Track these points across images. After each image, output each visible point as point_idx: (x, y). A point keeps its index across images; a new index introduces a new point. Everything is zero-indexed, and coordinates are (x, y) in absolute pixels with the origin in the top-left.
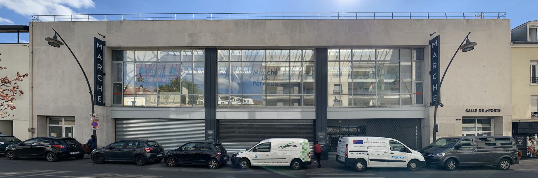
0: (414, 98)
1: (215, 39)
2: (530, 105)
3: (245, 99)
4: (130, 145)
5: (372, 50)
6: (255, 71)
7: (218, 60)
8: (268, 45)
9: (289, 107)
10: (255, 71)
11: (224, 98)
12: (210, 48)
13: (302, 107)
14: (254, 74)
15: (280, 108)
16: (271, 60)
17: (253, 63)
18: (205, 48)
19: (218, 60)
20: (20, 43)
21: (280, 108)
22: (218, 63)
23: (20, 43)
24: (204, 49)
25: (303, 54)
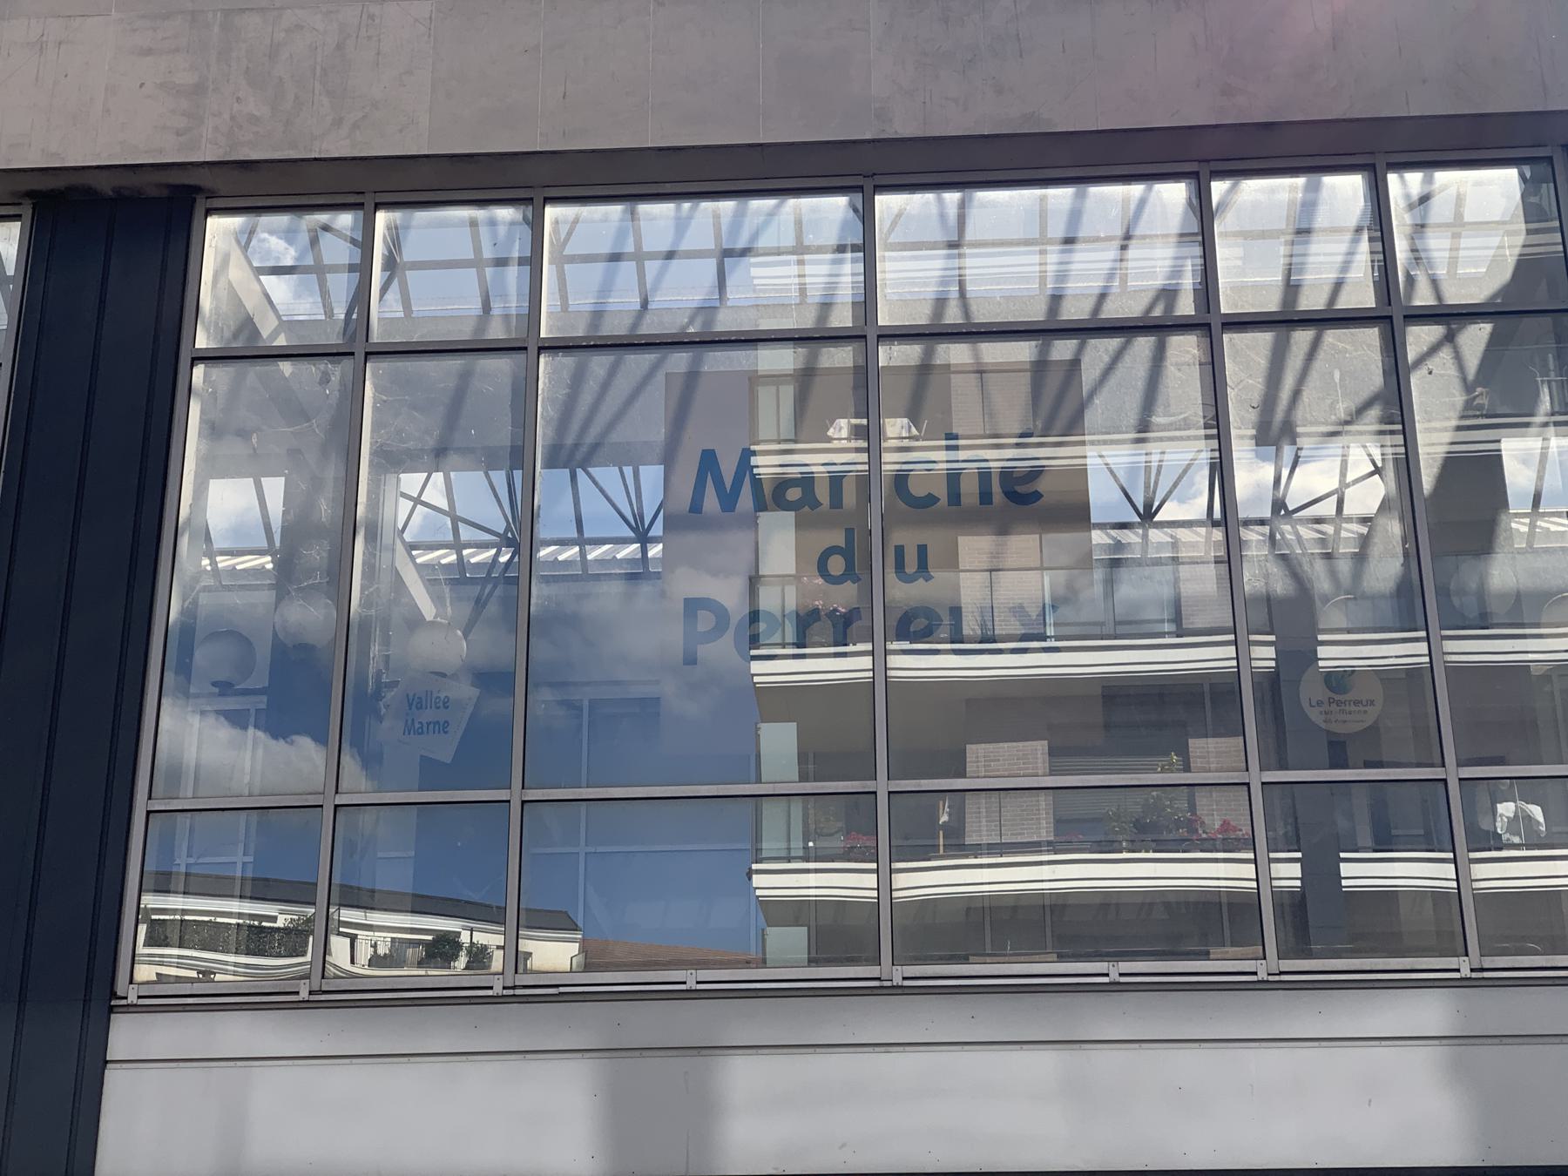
0: (1132, 779)
1: (186, 78)
2: (364, 780)
3: (481, 938)
4: (1347, 530)
5: (1344, 551)
6: (709, 461)
7: (202, 342)
8: (904, 126)
9: (1262, 970)
10: (709, 461)
11: (169, 912)
12: (105, 185)
13: (1465, 966)
14: (696, 507)
15: (1114, 988)
16: (962, 205)
17: (679, 360)
18: (30, 194)
19: (202, 342)
20: (1272, 865)
21: (1114, 988)
22: (199, 371)
23: (1272, 865)
24: (27, 211)
25: (1400, 220)
